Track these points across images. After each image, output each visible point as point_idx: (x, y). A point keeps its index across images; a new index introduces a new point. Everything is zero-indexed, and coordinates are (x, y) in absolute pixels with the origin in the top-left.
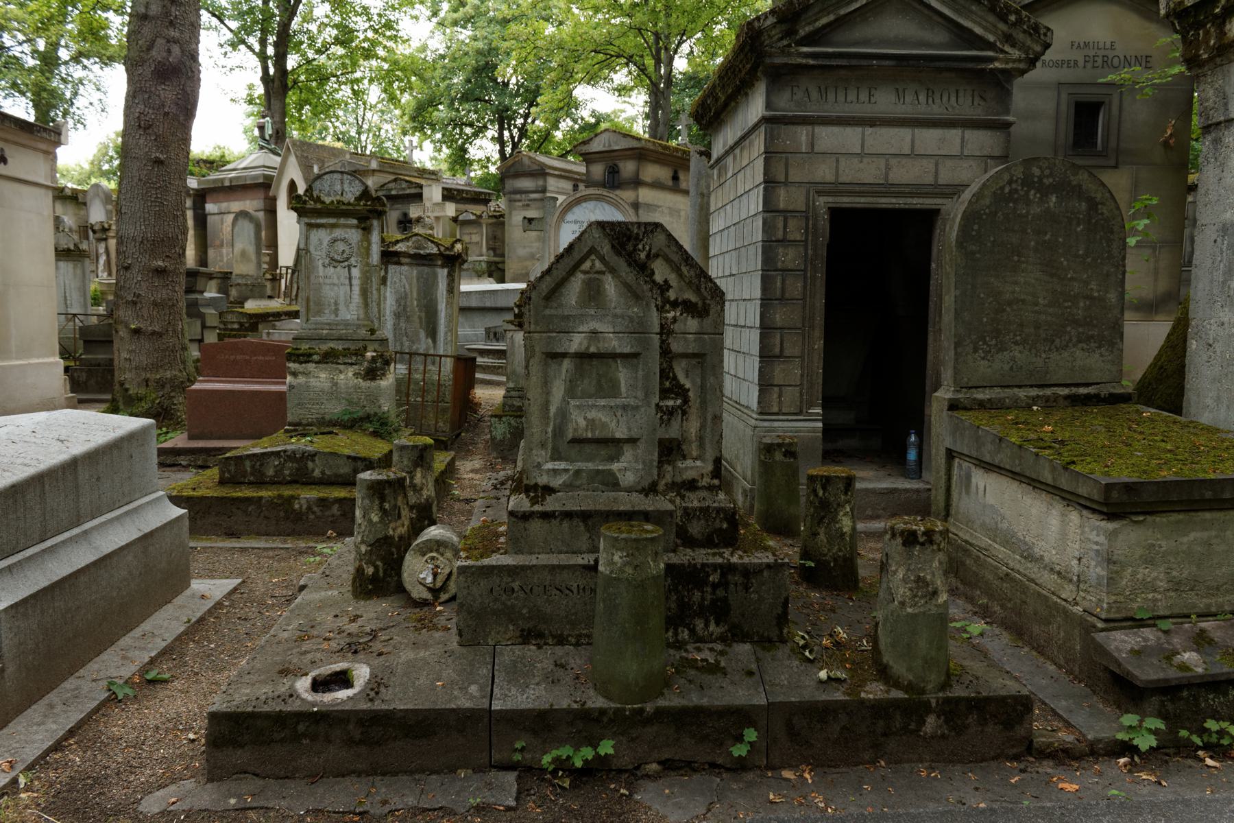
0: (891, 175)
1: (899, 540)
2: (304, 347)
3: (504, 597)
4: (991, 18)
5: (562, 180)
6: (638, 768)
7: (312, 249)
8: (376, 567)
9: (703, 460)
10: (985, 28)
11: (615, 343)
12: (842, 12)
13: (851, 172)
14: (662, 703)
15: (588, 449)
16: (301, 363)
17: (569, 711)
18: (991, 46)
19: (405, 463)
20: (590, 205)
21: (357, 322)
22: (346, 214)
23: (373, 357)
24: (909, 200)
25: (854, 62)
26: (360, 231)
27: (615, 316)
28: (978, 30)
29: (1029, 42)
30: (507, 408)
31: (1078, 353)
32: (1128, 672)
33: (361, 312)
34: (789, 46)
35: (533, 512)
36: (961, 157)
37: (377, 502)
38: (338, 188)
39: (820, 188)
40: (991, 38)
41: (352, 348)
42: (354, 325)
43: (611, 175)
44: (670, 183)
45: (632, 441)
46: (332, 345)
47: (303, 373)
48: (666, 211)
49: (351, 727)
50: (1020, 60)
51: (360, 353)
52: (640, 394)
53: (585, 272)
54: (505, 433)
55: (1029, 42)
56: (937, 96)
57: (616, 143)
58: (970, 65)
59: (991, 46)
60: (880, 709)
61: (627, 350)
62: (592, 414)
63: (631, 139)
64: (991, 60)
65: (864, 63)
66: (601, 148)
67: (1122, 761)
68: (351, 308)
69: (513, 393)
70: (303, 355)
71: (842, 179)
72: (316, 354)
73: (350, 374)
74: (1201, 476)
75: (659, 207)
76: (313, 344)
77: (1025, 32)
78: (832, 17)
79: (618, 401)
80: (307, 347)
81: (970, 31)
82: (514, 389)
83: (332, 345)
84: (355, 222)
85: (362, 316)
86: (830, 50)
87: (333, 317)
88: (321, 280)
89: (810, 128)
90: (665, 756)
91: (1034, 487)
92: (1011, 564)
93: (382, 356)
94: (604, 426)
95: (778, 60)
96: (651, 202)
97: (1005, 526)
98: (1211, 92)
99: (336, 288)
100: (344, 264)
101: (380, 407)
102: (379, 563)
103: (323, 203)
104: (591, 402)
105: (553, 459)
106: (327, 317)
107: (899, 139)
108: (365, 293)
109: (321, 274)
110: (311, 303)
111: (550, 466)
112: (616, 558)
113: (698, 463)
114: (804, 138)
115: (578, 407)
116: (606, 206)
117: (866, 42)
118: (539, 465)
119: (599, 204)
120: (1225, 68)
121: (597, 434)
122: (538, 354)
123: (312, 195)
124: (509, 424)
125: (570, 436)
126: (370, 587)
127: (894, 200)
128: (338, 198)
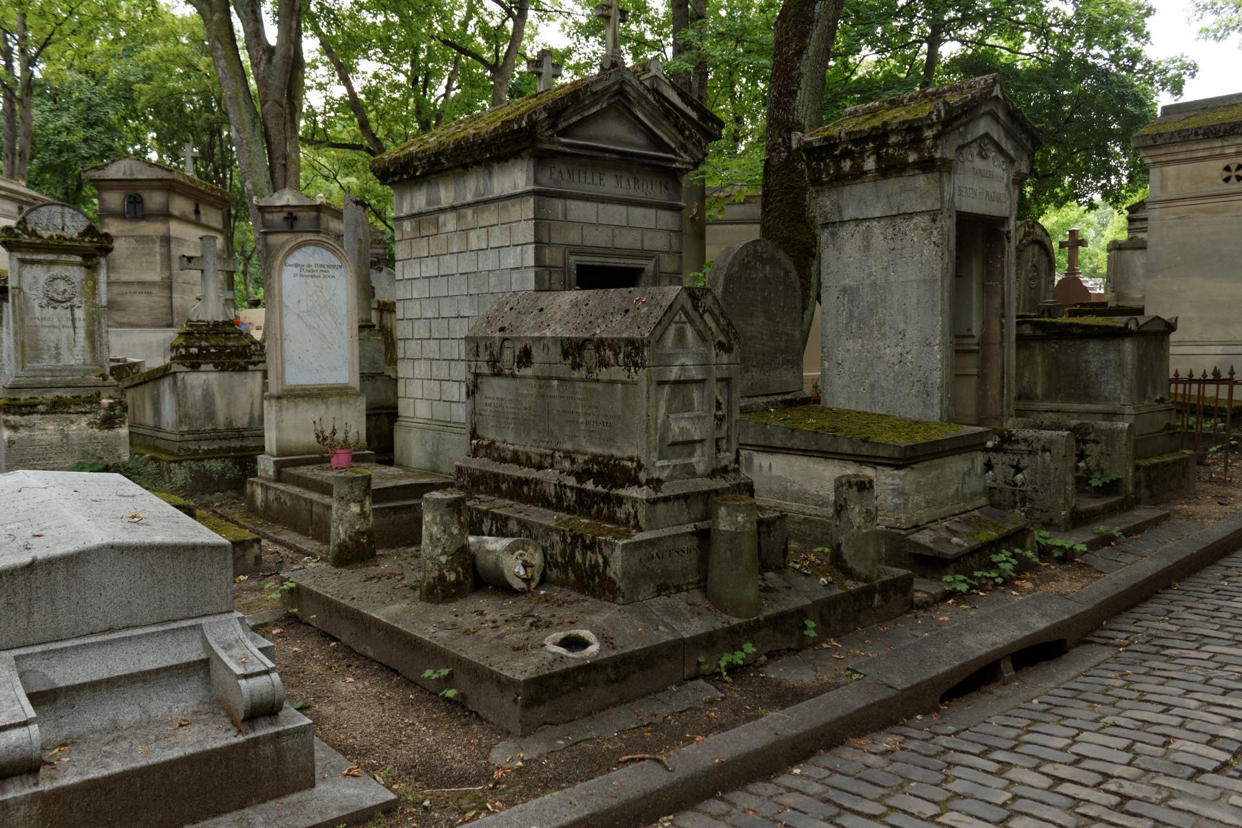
0: (616, 242)
1: (855, 488)
2: (24, 396)
3: (648, 564)
4: (674, 131)
5: (7, 202)
6: (755, 661)
7: (25, 287)
8: (458, 573)
9: (730, 452)
10: (670, 138)
11: (694, 372)
12: (586, 114)
13: (598, 238)
14: (766, 613)
15: (678, 449)
16: (23, 414)
17: (724, 629)
18: (672, 151)
19: (357, 493)
20: (310, 249)
21: (83, 367)
22: (69, 250)
23: (110, 404)
24: (626, 261)
25: (595, 154)
26: (83, 269)
27: (694, 353)
28: (666, 139)
29: (695, 151)
30: (183, 453)
31: (783, 372)
32: (939, 553)
33: (88, 357)
34: (552, 136)
35: (659, 498)
36: (656, 230)
37: (456, 517)
38: (58, 221)
39: (572, 249)
40: (673, 146)
41: (83, 395)
42: (80, 370)
43: (132, 206)
44: (193, 217)
45: (701, 441)
46: (59, 393)
47: (26, 426)
48: (192, 246)
49: (609, 670)
50: (689, 163)
51: (94, 400)
52: (706, 407)
53: (676, 323)
54: (186, 478)
55: (695, 151)
56: (640, 182)
57: (140, 172)
58: (662, 164)
59: (672, 151)
60: (856, 596)
61: (700, 377)
62: (683, 424)
63: (160, 170)
64: (674, 161)
65: (601, 155)
66: (120, 176)
67: (950, 602)
68: (76, 352)
69: (187, 437)
70: (25, 406)
71: (587, 243)
72: (41, 403)
73: (84, 424)
74: (934, 438)
75: (186, 241)
76: (35, 393)
77: (693, 143)
78: (579, 117)
79: (693, 414)
80: (28, 396)
81: (660, 138)
82: (188, 433)
83: (59, 393)
84: (79, 259)
85: (88, 361)
86: (580, 142)
87: (53, 362)
88: (38, 322)
89: (563, 201)
90: (769, 649)
91: (826, 458)
92: (808, 512)
93: (120, 402)
94: (688, 431)
95: (546, 146)
96: (179, 236)
97: (796, 487)
98: (828, 202)
99: (56, 331)
100: (64, 305)
101: (119, 457)
102: (459, 569)
103: (40, 237)
104: (681, 415)
105: (660, 459)
106: (47, 362)
107: (617, 214)
108: (91, 336)
109: (38, 315)
110: (27, 348)
111: (659, 464)
112: (740, 519)
113: (728, 454)
114: (560, 209)
115: (675, 419)
116: (324, 251)
117: (597, 139)
118: (654, 464)
119: (318, 250)
120: (840, 189)
121: (685, 438)
122: (654, 383)
123: (26, 228)
124: (190, 468)
125: (670, 441)
126: (453, 591)
127: (617, 260)
128: (58, 232)
